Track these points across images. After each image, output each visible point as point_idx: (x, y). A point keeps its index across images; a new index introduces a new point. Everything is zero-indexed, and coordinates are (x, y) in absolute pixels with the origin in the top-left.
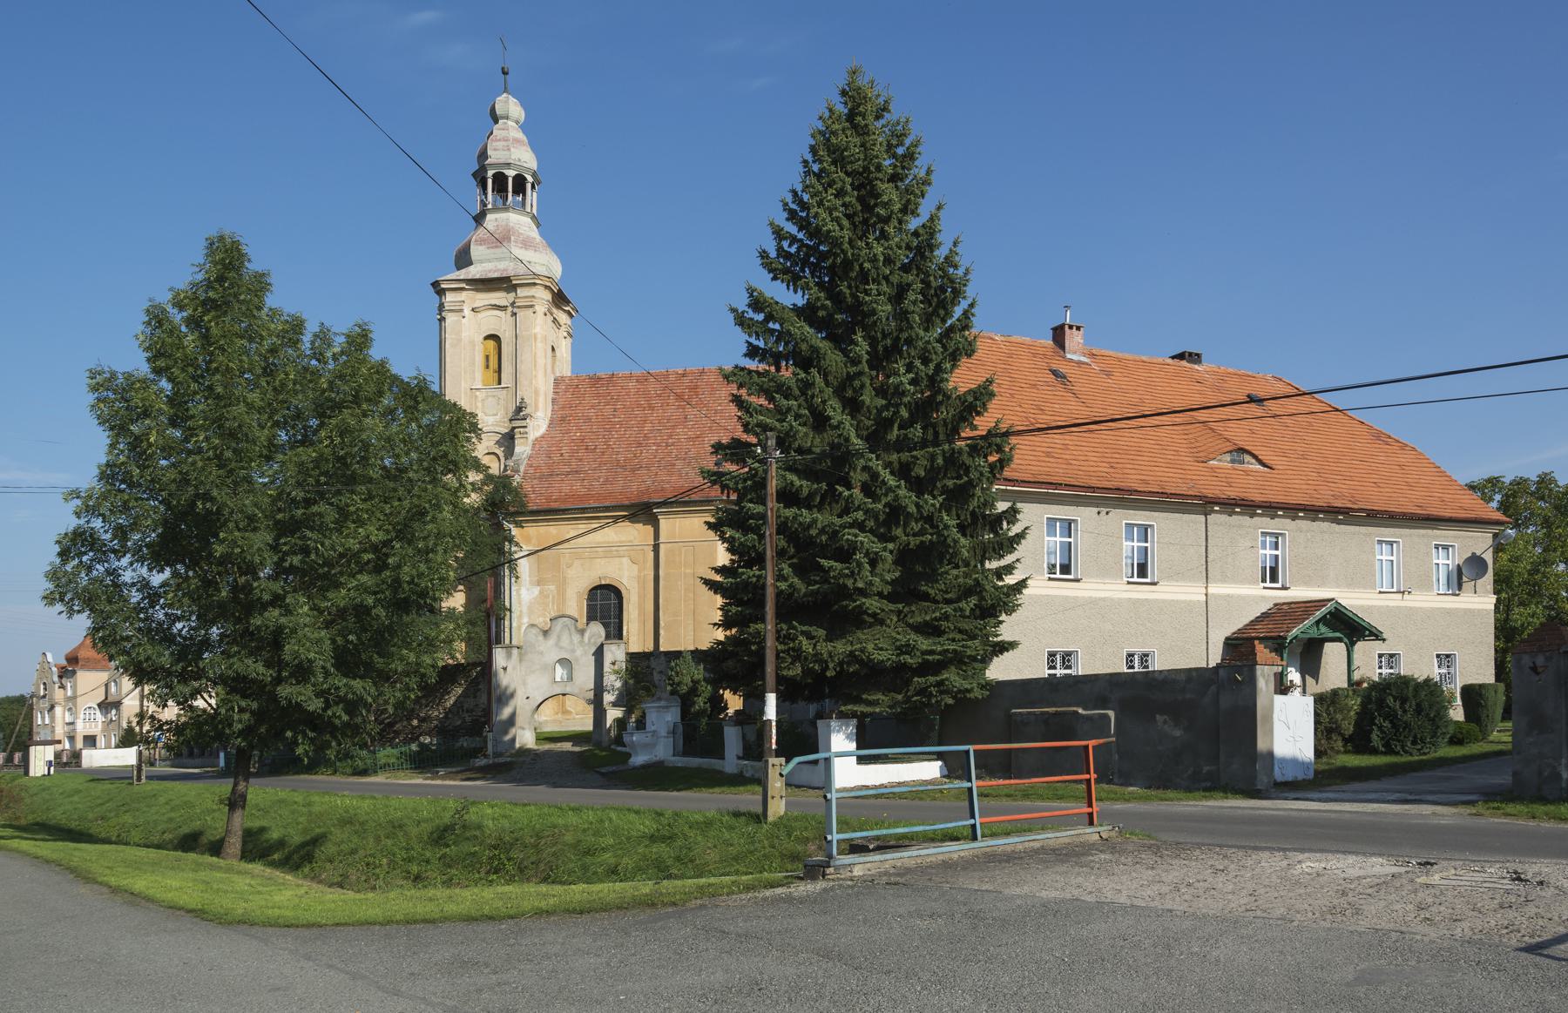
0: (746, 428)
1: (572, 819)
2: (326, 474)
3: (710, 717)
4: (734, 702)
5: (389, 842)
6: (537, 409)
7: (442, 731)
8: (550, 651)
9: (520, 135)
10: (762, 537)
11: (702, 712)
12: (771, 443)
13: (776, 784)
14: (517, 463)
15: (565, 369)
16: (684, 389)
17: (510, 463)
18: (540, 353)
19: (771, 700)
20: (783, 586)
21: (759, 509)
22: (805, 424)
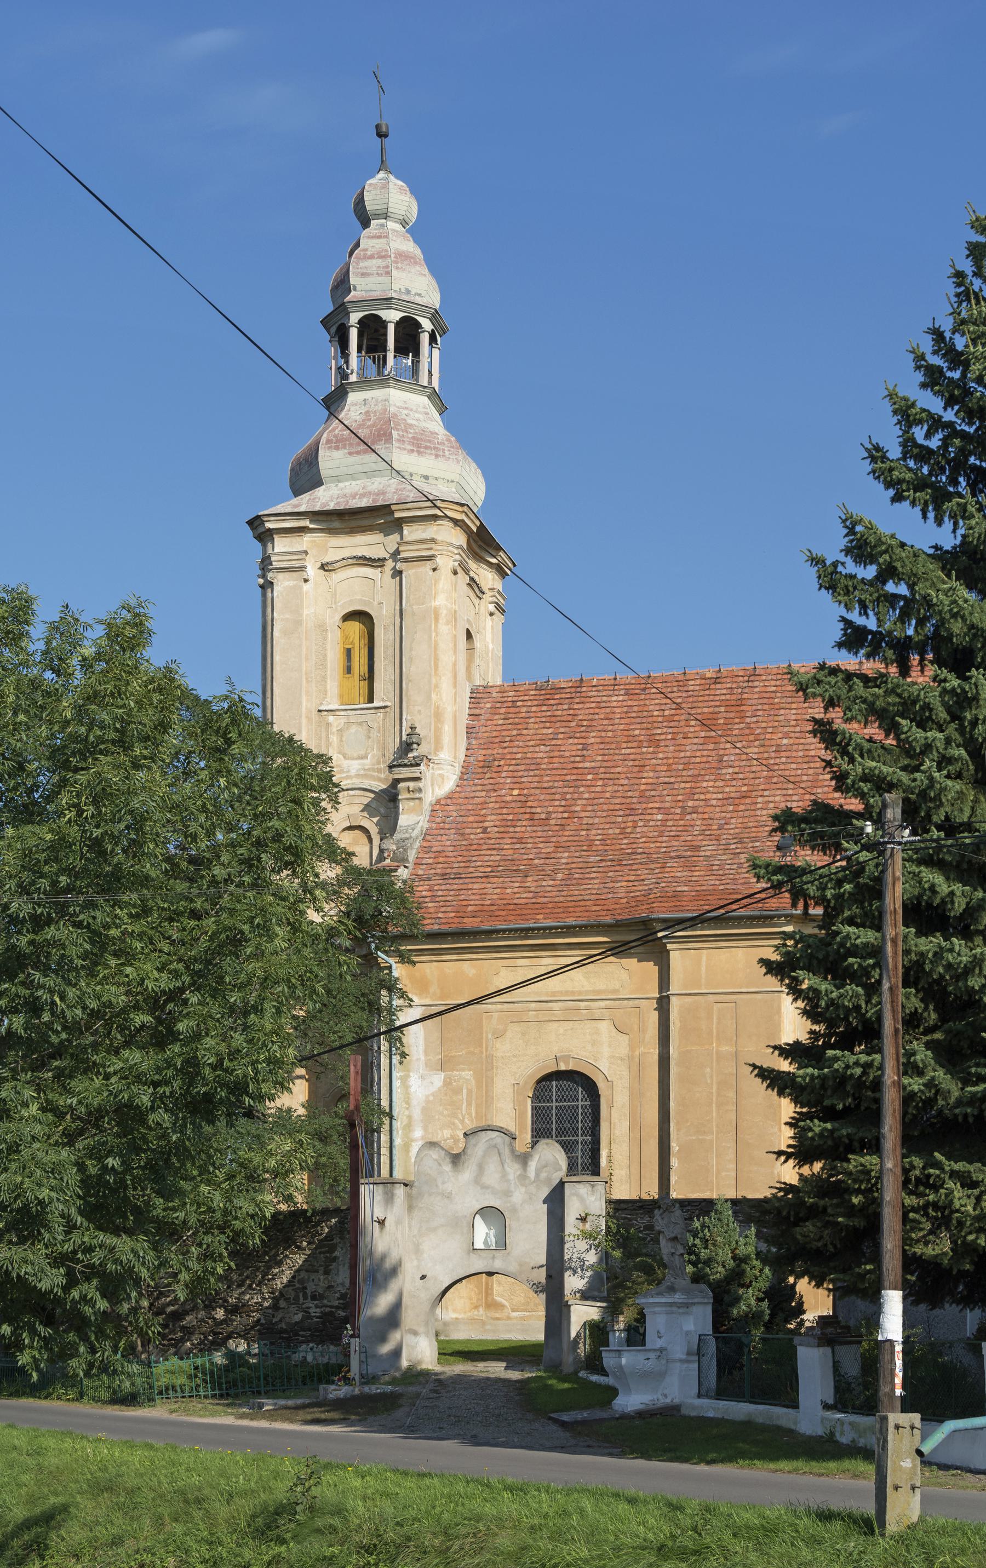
0: (841, 780)
1: (510, 1505)
2: (68, 871)
3: (768, 1326)
4: (816, 1302)
5: (179, 1529)
6: (438, 747)
7: (266, 1330)
8: (463, 1192)
9: (410, 246)
10: (873, 989)
11: (753, 1318)
12: (894, 814)
13: (902, 1463)
14: (403, 845)
15: (491, 672)
16: (716, 706)
17: (390, 845)
18: (445, 645)
19: (893, 1304)
20: (915, 1084)
21: (867, 936)
22: (959, 776)
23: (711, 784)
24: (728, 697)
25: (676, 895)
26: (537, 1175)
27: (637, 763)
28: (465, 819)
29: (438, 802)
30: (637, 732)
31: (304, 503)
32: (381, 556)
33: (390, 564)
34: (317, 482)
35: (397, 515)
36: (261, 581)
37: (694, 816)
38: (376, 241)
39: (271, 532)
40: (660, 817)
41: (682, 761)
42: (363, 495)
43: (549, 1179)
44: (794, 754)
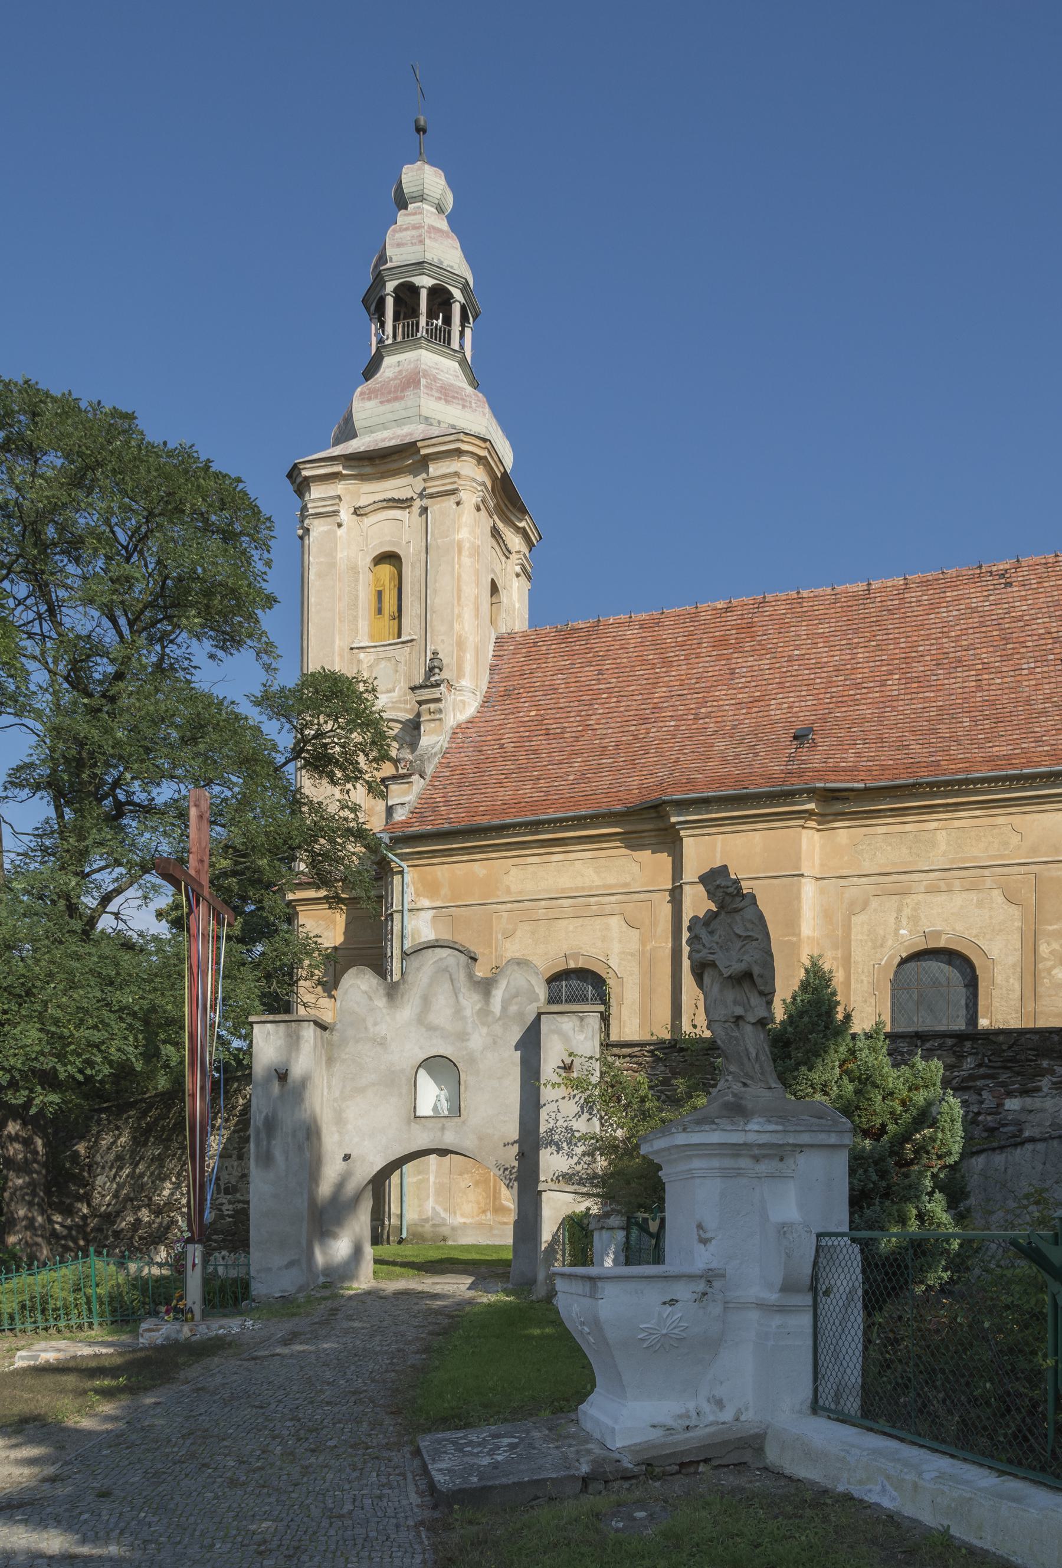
6: (460, 675)
23: (723, 692)
24: (739, 622)
25: (689, 781)
26: (504, 1008)
27: (650, 681)
28: (483, 739)
29: (459, 726)
30: (651, 657)
32: (409, 497)
33: (418, 503)
35: (423, 452)
37: (707, 720)
39: (307, 480)
40: (672, 723)
41: (695, 676)
42: (392, 439)
43: (521, 1014)
44: (806, 662)
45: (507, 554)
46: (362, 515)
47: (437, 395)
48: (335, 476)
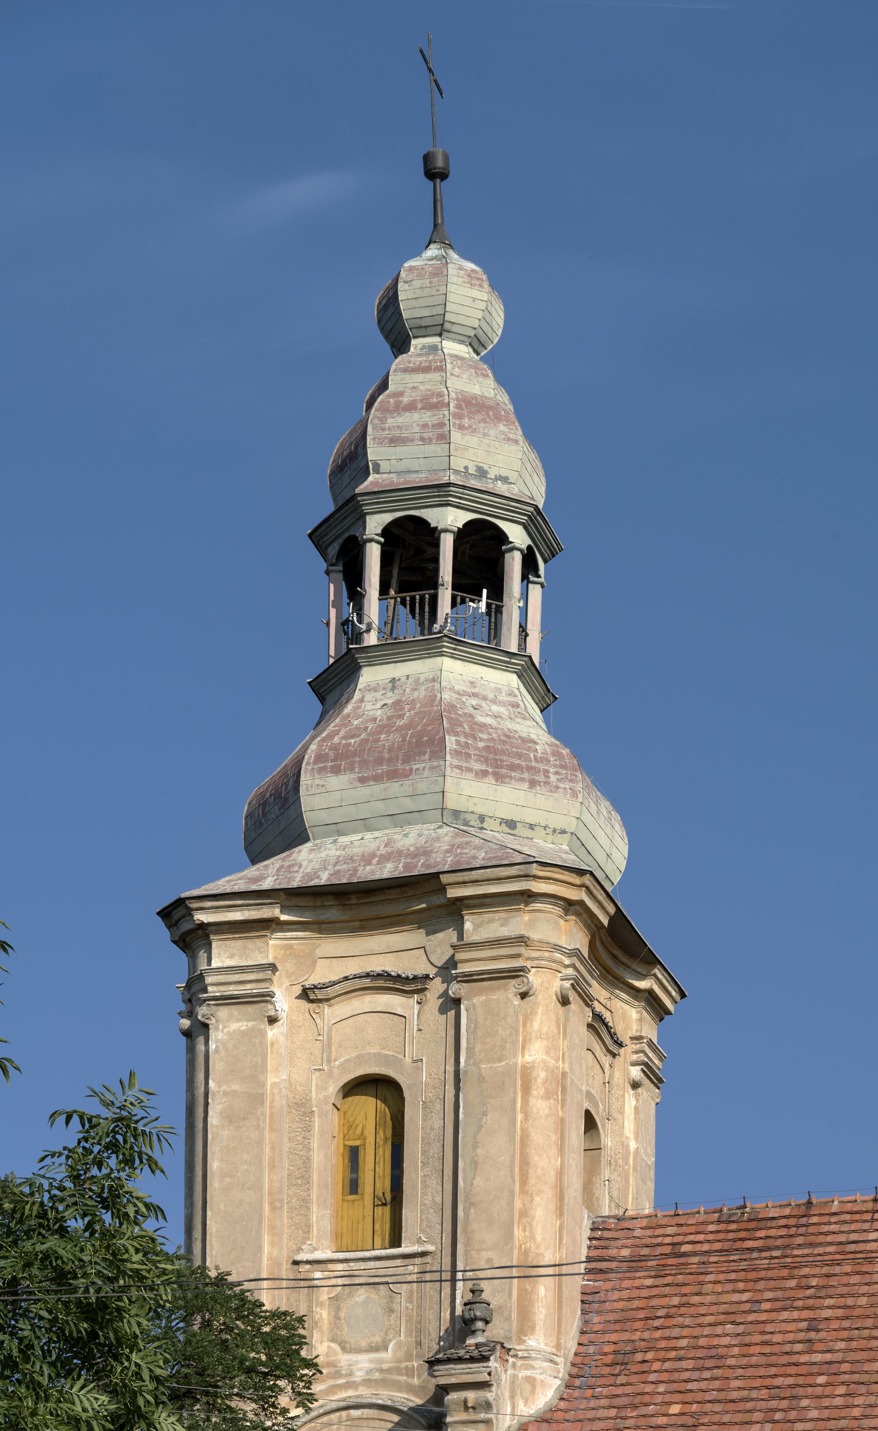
6: (526, 1326)
9: (485, 387)
15: (632, 1191)
31: (270, 874)
33: (437, 986)
34: (297, 835)
36: (186, 1023)
38: (420, 377)
39: (204, 932)
45: (614, 1048)
46: (320, 1001)
47: (478, 767)
48: (267, 925)
